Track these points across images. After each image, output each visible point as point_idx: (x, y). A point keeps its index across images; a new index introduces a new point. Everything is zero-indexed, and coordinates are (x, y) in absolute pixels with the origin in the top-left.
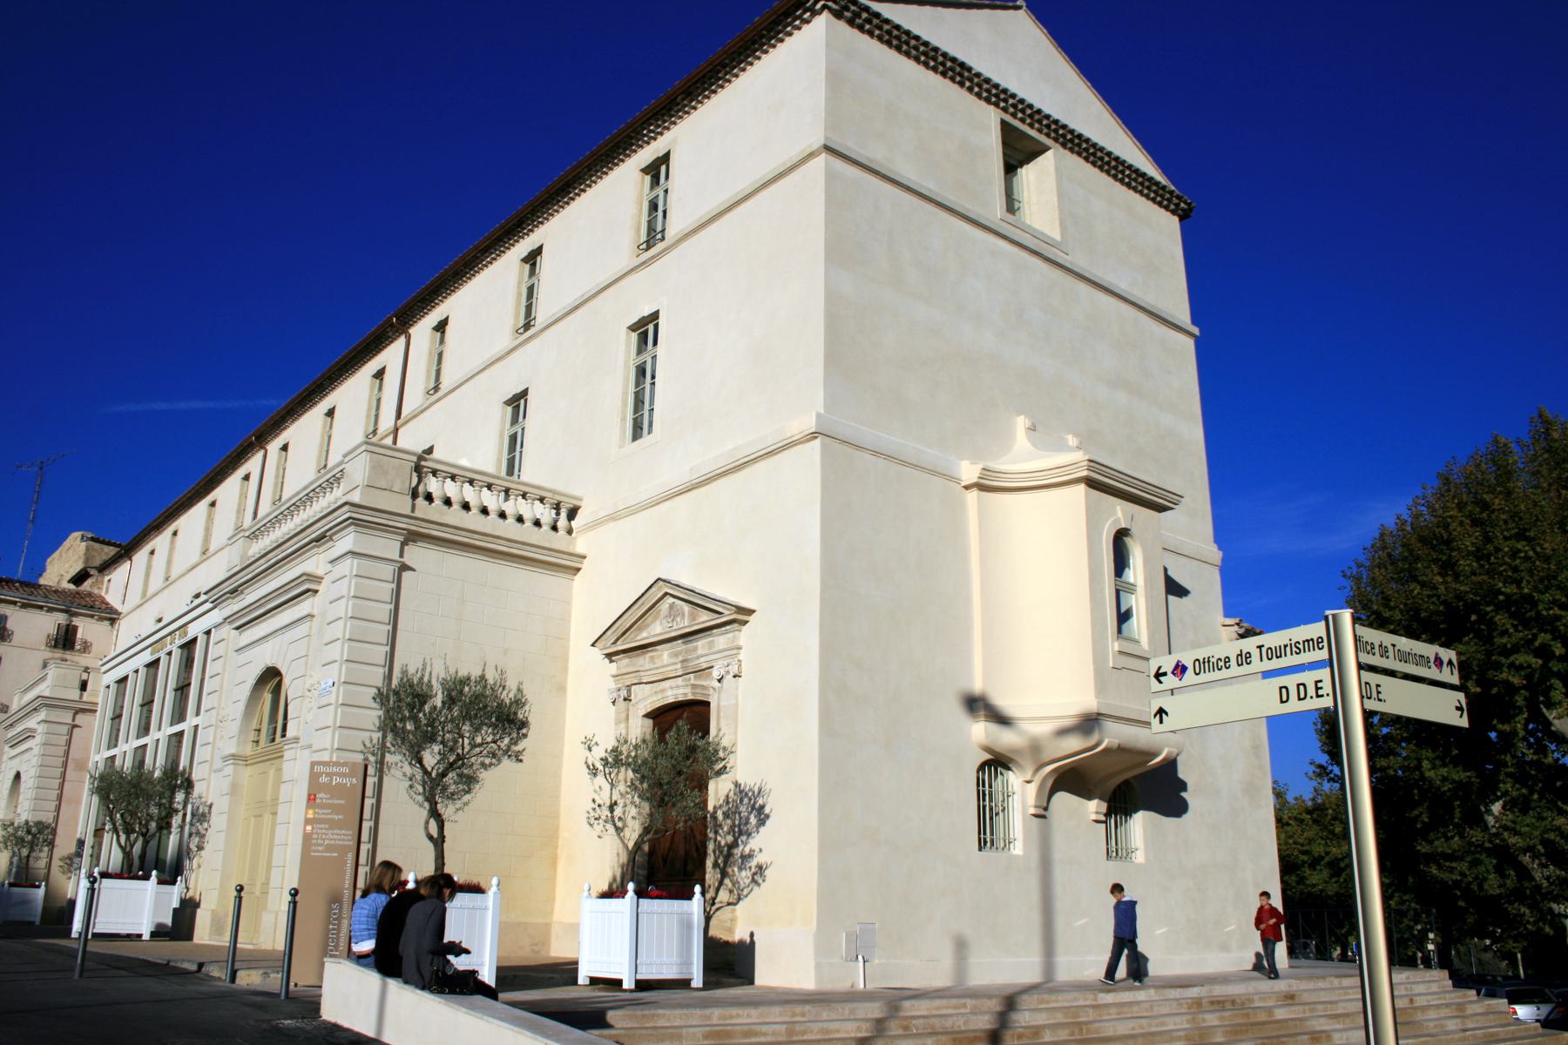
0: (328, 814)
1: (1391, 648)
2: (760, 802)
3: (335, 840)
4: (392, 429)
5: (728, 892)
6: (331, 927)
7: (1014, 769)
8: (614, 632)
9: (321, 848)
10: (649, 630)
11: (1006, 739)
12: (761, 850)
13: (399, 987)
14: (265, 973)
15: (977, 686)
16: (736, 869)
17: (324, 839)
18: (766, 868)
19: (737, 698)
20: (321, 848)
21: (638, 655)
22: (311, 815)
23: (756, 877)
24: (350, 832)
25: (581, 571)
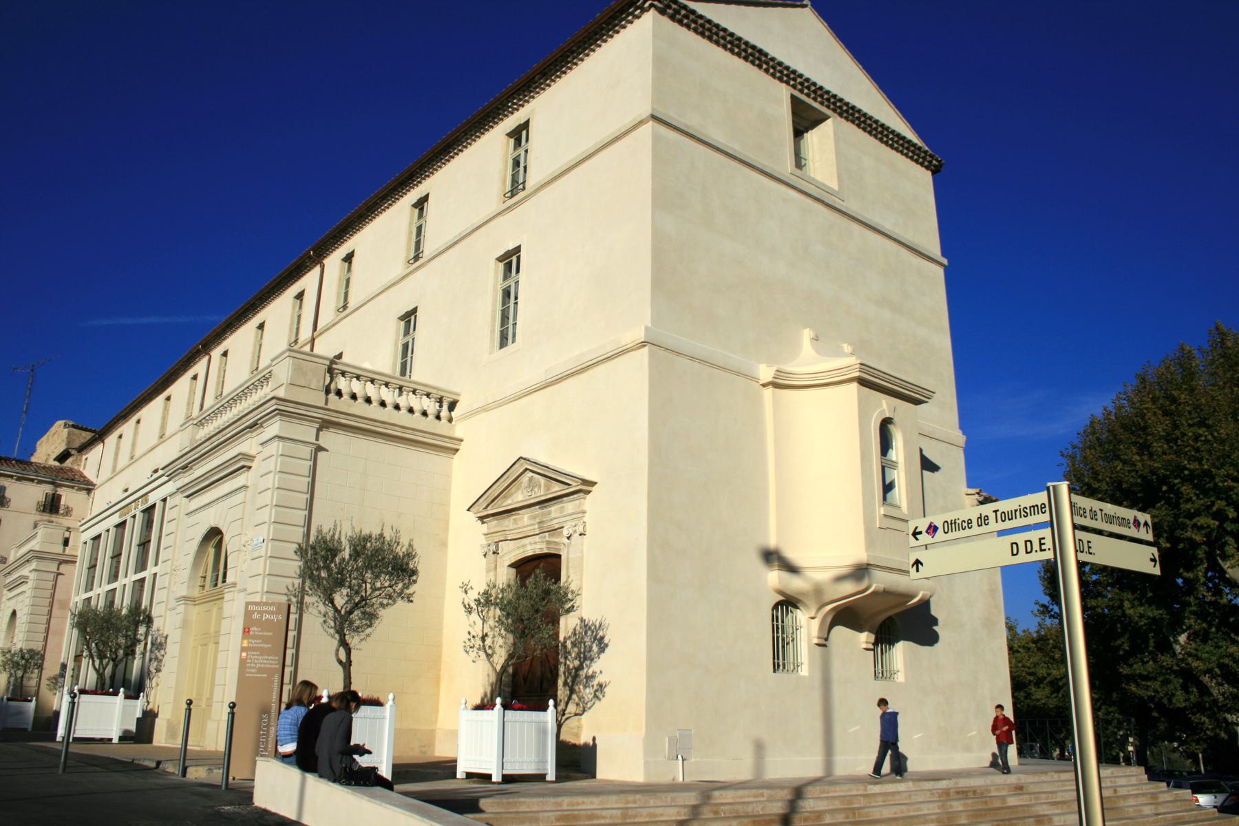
0: (260, 643)
2: (601, 634)
3: (264, 664)
4: (310, 339)
5: (575, 705)
6: (261, 732)
7: (801, 608)
8: (485, 500)
9: (253, 671)
10: (513, 497)
11: (795, 584)
12: (601, 672)
13: (315, 781)
14: (210, 769)
15: (772, 542)
16: (581, 687)
17: (256, 663)
18: (605, 687)
19: (582, 552)
20: (253, 671)
21: (504, 518)
22: (245, 644)
23: (597, 693)
24: (277, 658)
25: (459, 452)
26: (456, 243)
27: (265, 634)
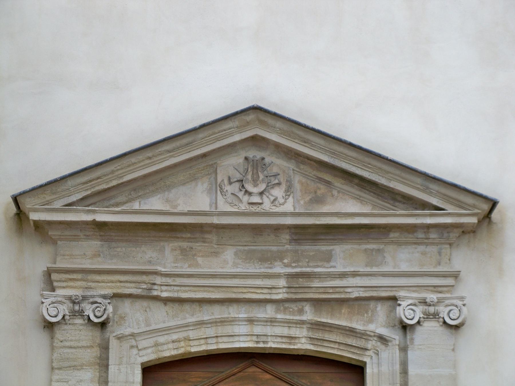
10: (172, 194)
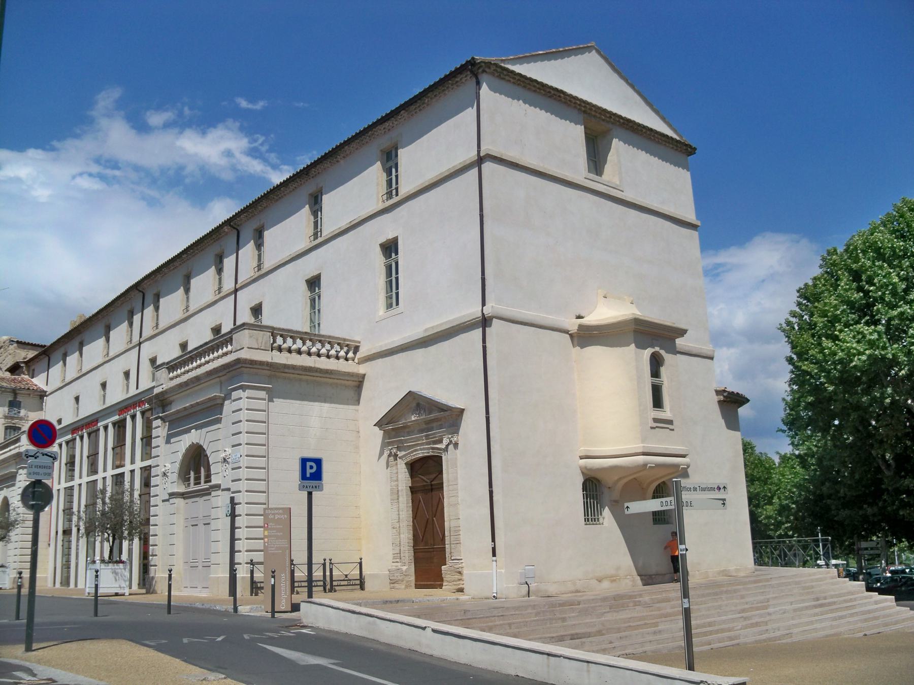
1: (698, 488)
4: (233, 289)
9: (273, 549)
17: (274, 545)
24: (286, 541)
26: (570, 659)
27: (278, 527)
